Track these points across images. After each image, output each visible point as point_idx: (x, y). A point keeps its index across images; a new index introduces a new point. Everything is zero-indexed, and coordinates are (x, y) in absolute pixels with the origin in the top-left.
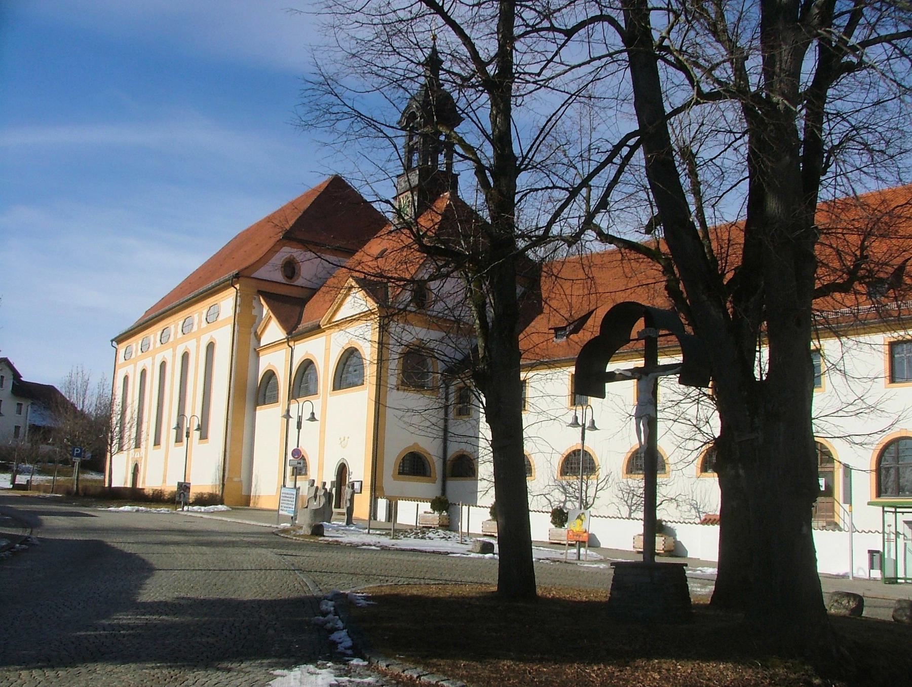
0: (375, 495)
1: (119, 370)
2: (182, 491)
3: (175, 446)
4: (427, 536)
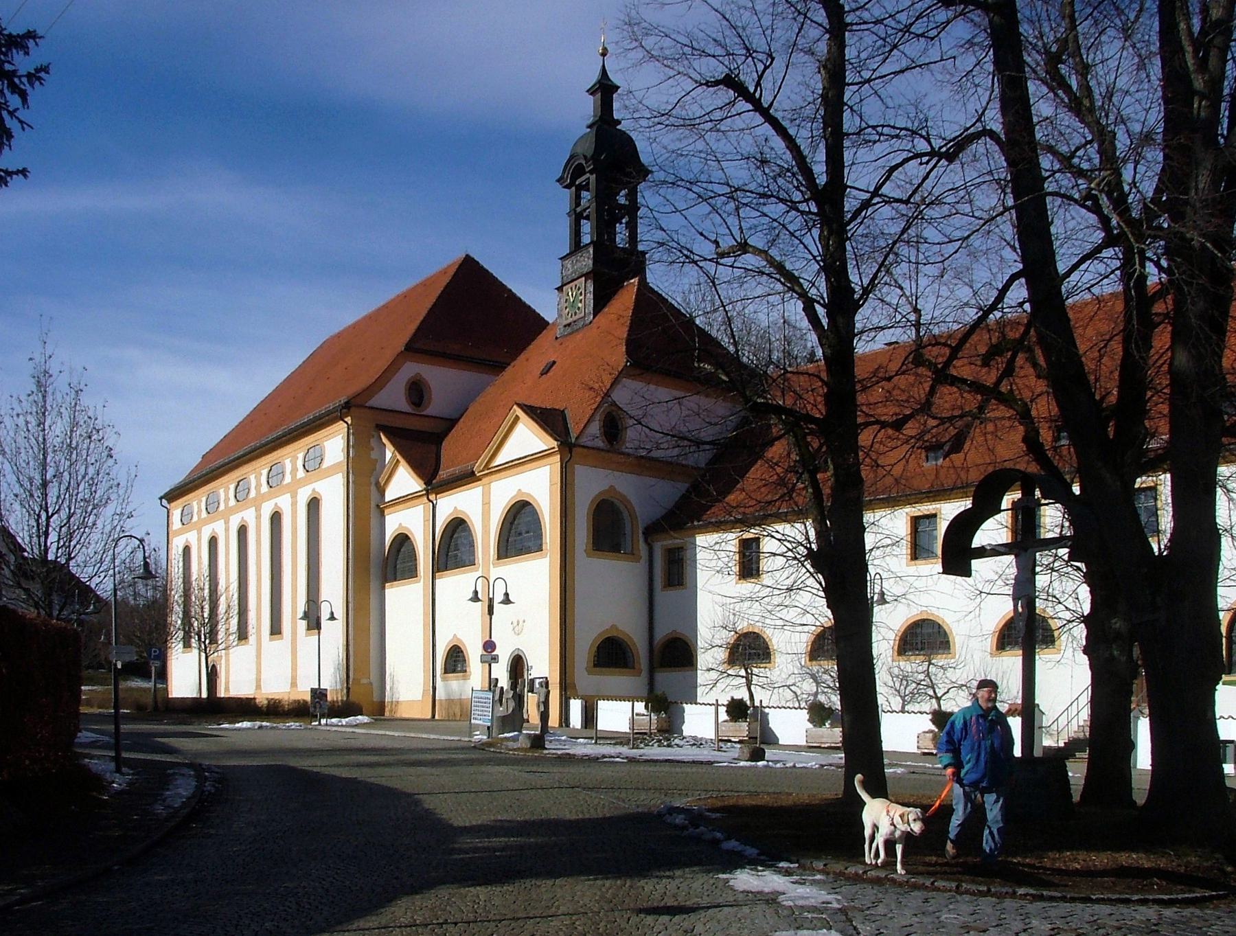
0: (566, 694)
1: (174, 539)
2: (317, 700)
3: (271, 640)
4: (673, 743)
